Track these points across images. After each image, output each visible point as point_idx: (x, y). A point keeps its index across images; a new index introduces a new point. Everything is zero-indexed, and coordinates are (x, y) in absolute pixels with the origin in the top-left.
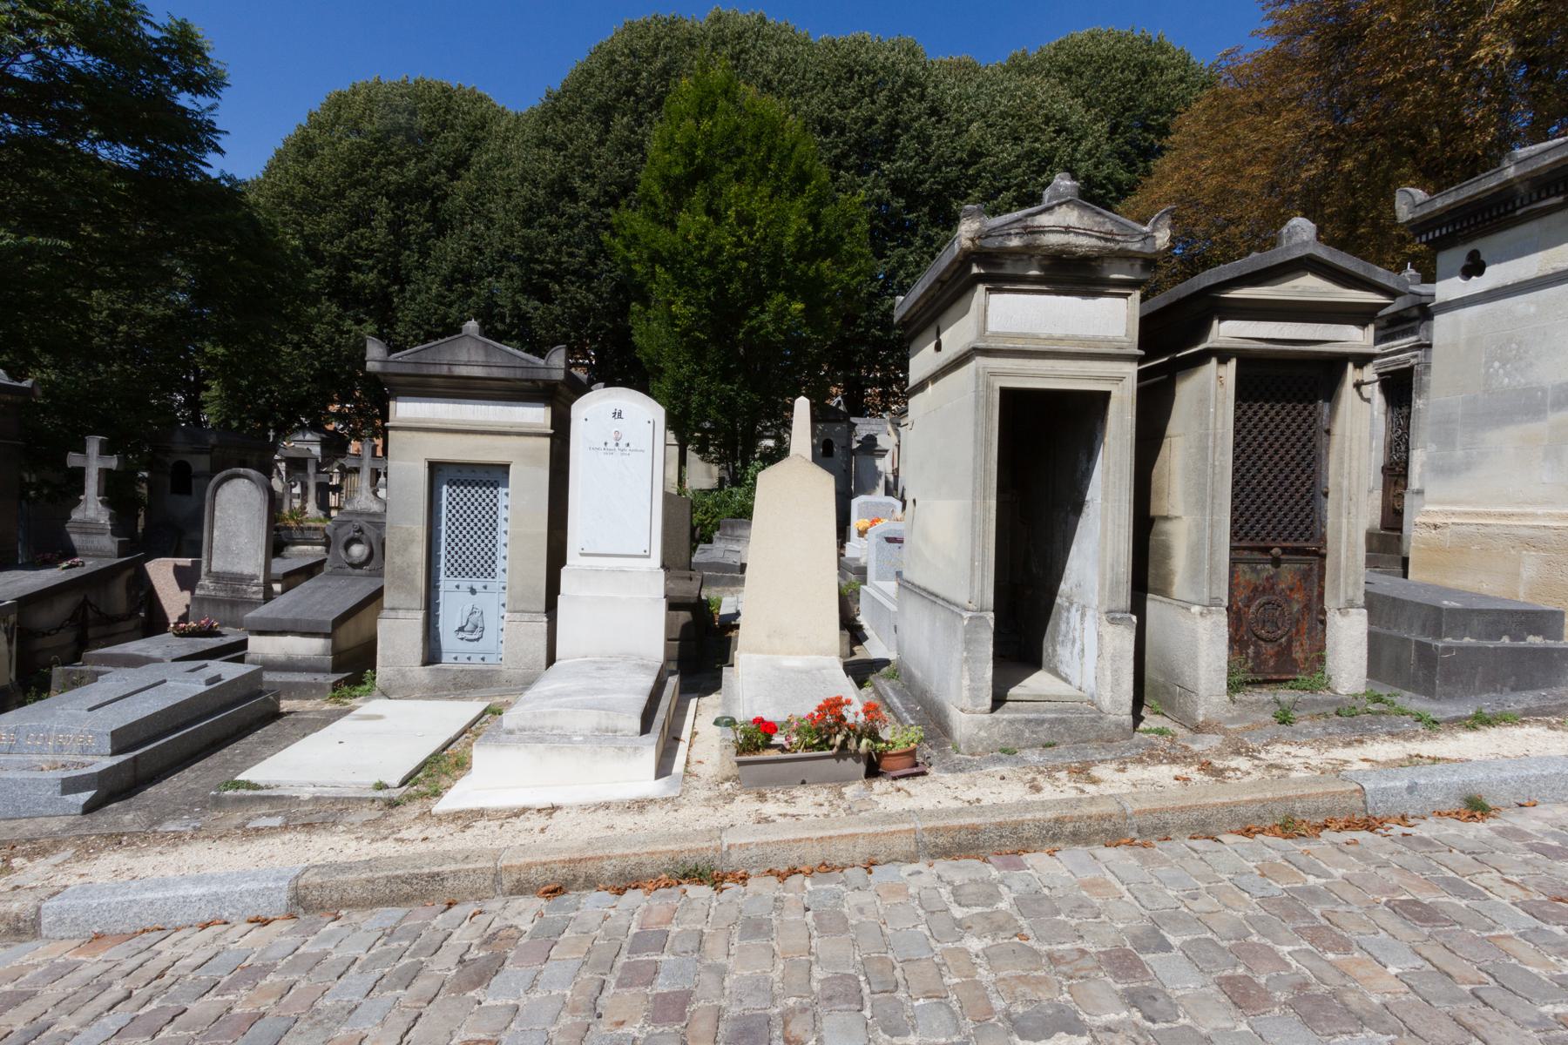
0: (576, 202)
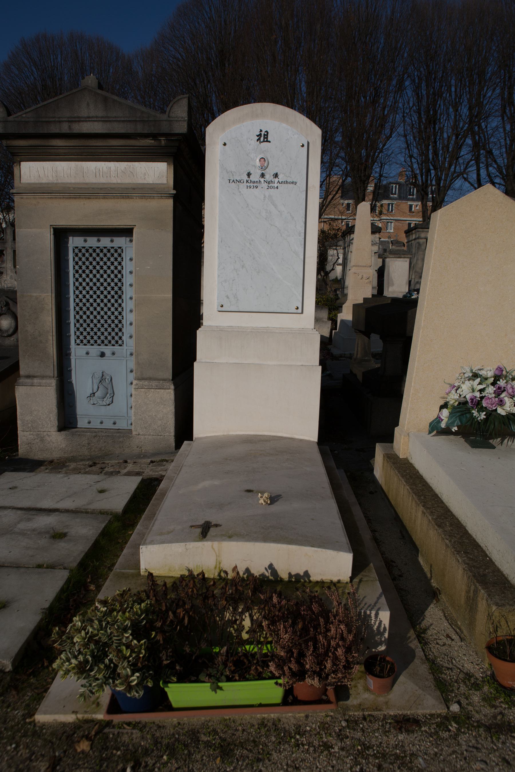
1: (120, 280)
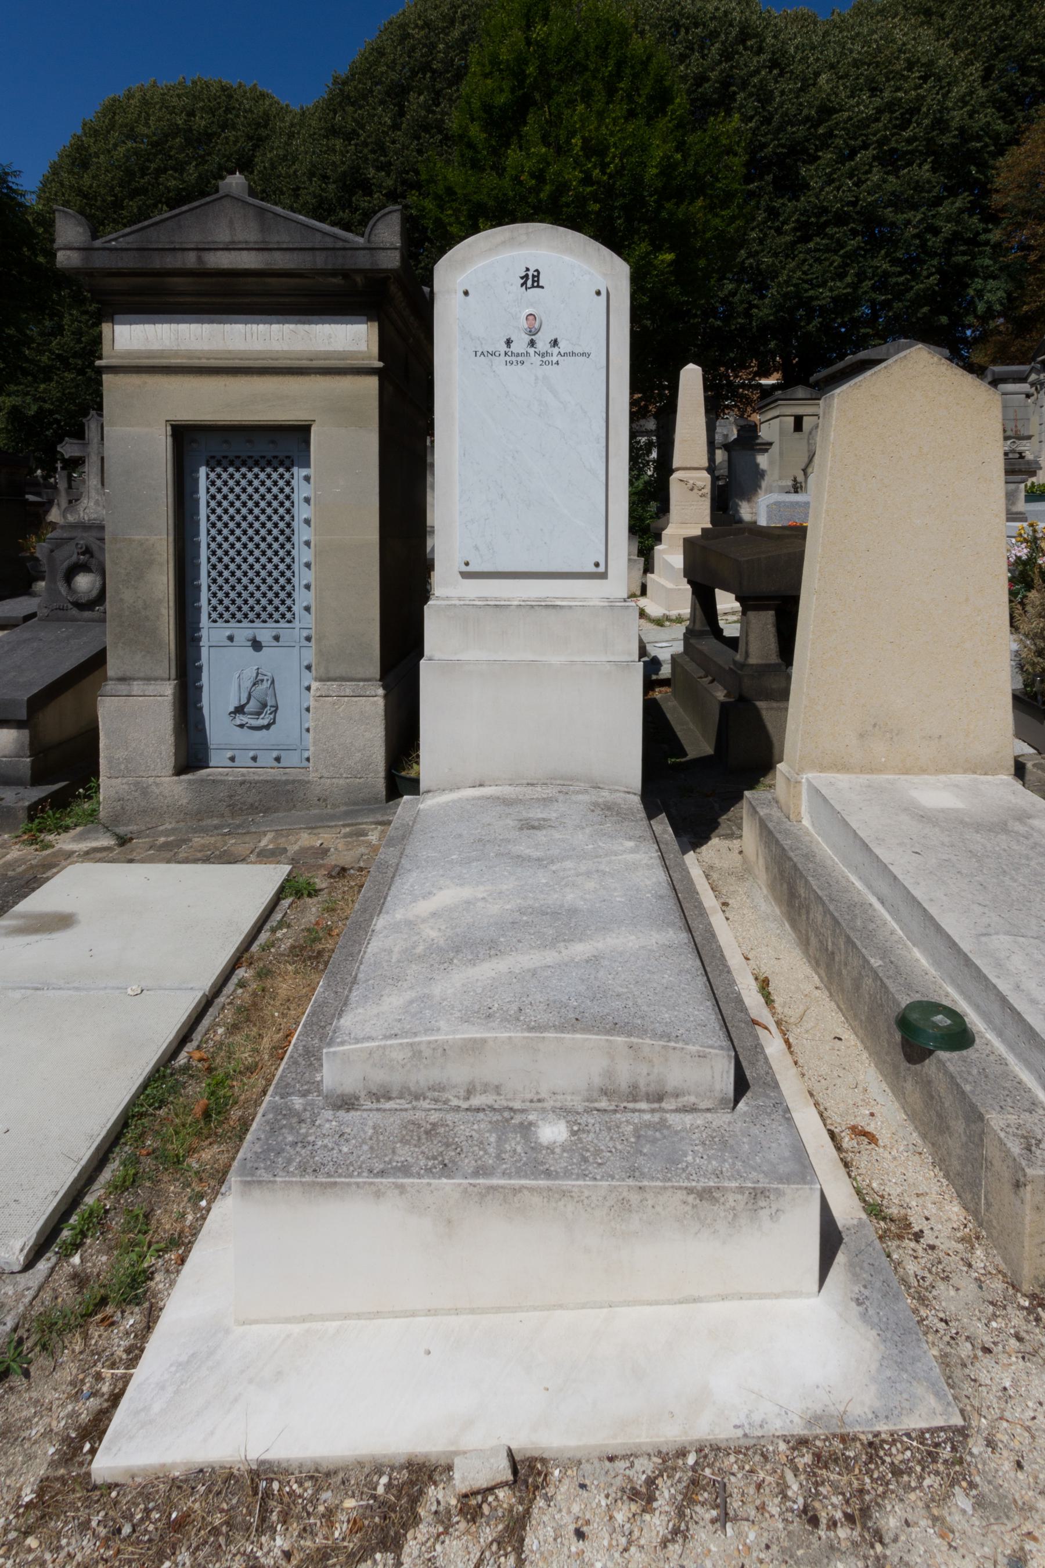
0: (370, 194)
1: (288, 511)
